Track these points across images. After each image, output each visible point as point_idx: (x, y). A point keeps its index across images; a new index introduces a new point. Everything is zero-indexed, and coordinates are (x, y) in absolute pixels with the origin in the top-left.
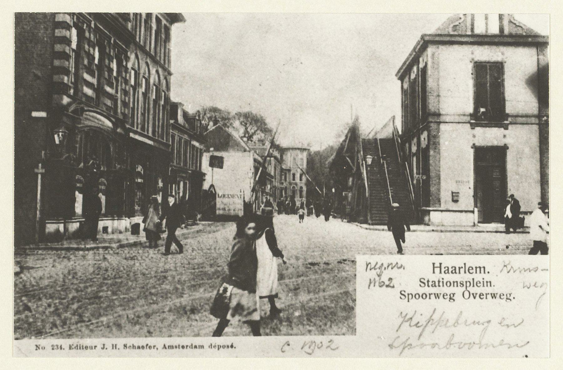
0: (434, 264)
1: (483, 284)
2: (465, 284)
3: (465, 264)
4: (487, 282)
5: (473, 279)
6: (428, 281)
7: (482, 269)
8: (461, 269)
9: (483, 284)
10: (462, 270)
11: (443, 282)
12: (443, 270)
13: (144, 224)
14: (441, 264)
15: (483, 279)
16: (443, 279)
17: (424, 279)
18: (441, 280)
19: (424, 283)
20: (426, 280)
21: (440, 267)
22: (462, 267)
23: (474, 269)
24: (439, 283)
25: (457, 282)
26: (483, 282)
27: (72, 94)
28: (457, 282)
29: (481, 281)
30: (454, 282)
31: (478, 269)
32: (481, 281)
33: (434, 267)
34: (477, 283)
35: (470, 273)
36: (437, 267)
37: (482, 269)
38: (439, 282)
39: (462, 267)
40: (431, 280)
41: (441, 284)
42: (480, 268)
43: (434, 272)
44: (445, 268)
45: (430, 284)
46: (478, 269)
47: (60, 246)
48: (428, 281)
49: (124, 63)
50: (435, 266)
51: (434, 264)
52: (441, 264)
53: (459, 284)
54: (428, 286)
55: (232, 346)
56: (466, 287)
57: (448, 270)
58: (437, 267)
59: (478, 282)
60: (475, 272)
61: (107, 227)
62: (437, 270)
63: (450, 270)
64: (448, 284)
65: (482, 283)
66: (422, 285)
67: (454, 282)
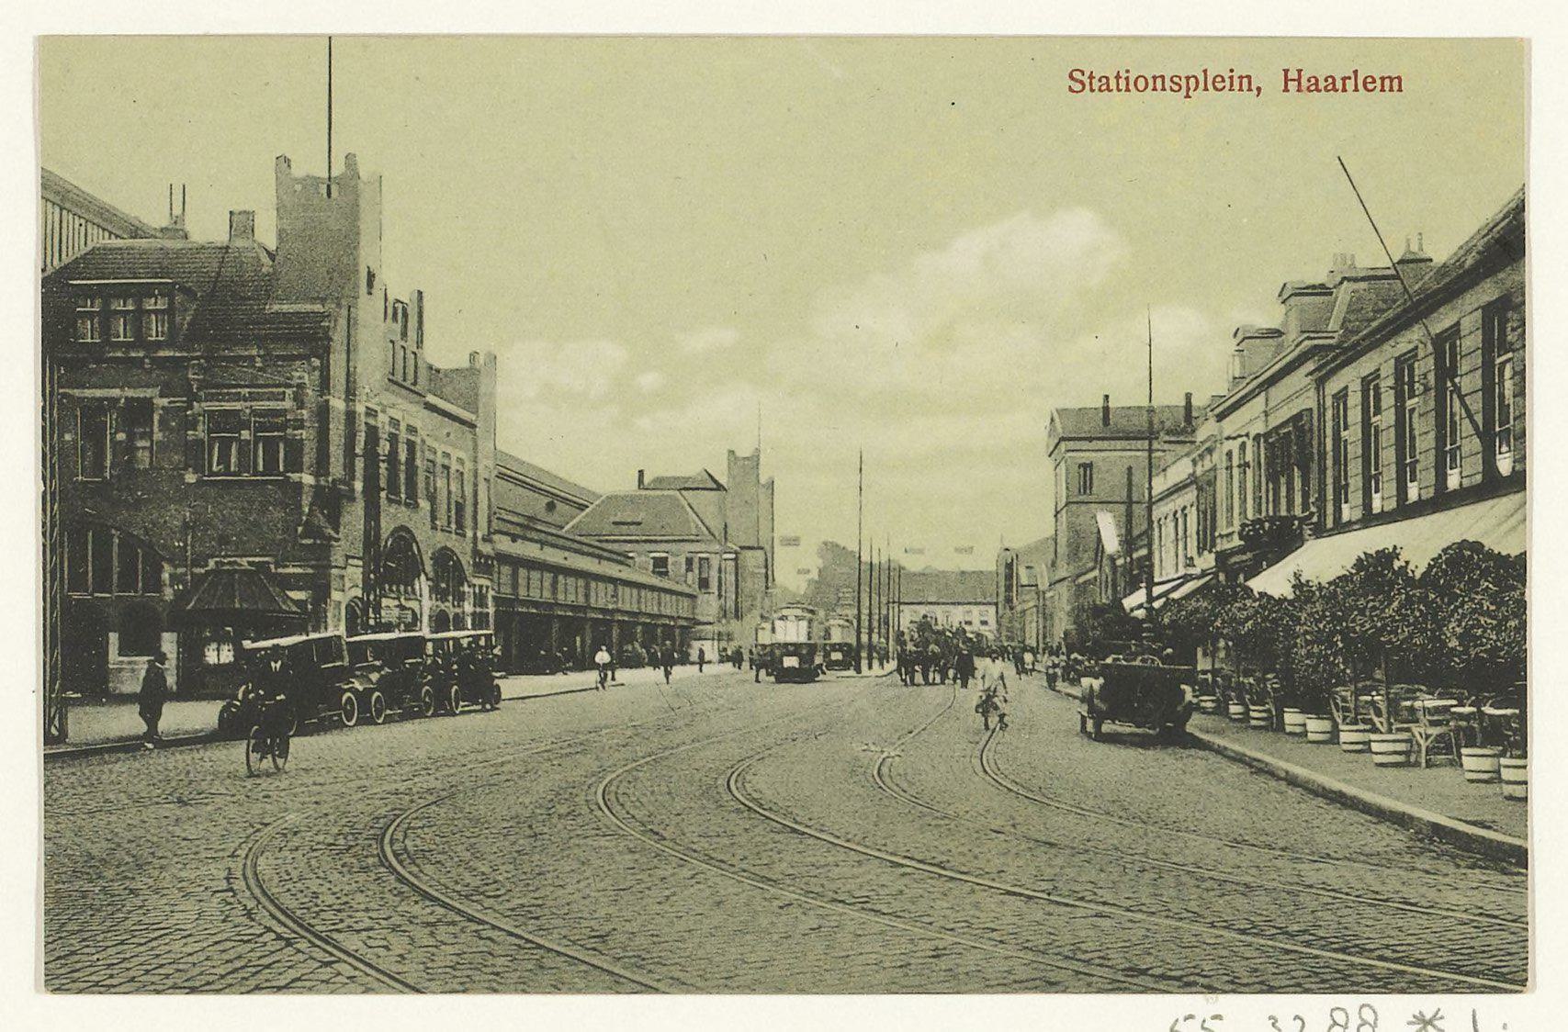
0: (1286, 71)
1: (1232, 85)
2: (1183, 83)
3: (1356, 72)
5: (1205, 71)
6: (1091, 77)
7: (1396, 81)
8: (1347, 81)
9: (1232, 85)
10: (1350, 84)
11: (1127, 78)
14: (1300, 71)
15: (1232, 71)
18: (1123, 75)
19: (1082, 82)
20: (1087, 74)
22: (1350, 78)
23: (1379, 82)
26: (1231, 78)
27: (1221, 640)
28: (1163, 77)
29: (1227, 75)
30: (1155, 78)
31: (1387, 82)
32: (1227, 75)
36: (1294, 80)
37: (1396, 81)
38: (1118, 77)
39: (1350, 78)
43: (1286, 90)
45: (1096, 85)
46: (1387, 82)
48: (1091, 77)
49: (291, 733)
51: (1286, 71)
52: (1300, 71)
53: (1168, 84)
54: (1119, 90)
55: (1420, 234)
56: (1188, 89)
57: (1334, 83)
58: (1294, 80)
59: (1219, 79)
60: (1379, 88)
62: (1293, 85)
64: (1141, 83)
66: (1078, 87)
67: (1155, 78)
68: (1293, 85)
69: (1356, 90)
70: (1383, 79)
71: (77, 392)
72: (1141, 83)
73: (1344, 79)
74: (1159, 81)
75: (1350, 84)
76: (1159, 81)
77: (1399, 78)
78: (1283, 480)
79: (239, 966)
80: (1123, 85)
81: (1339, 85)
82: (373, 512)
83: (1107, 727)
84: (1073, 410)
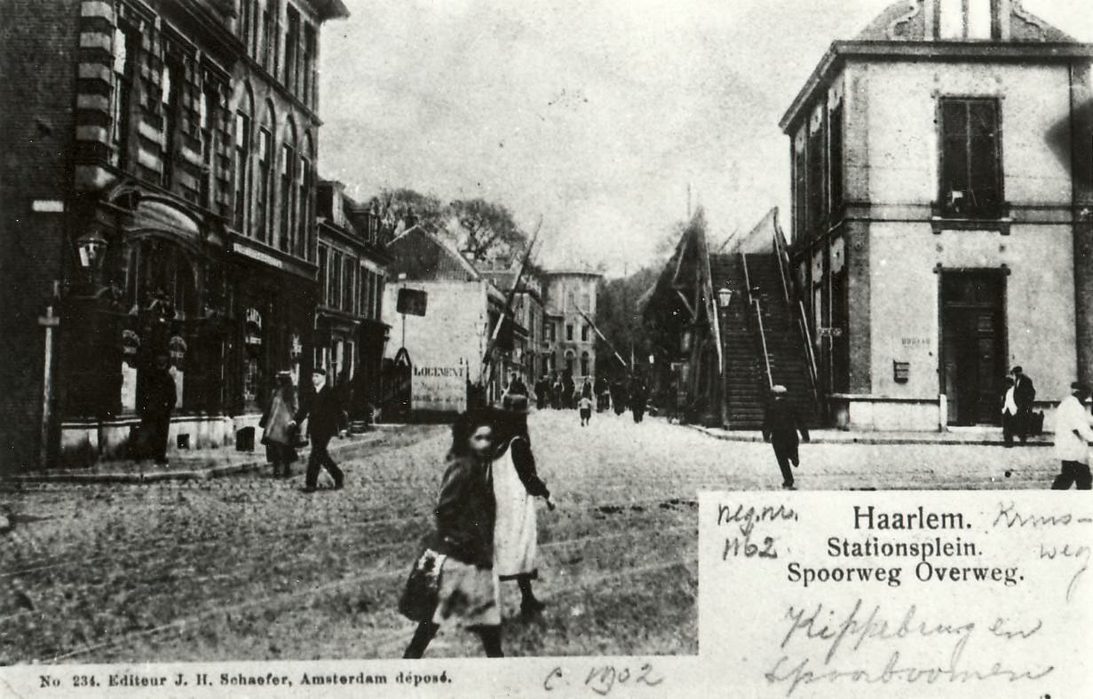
0: (857, 509)
3: (921, 509)
4: (966, 546)
5: (938, 540)
6: (846, 544)
7: (956, 520)
10: (915, 522)
11: (876, 546)
12: (876, 521)
13: (262, 430)
14: (871, 509)
15: (959, 539)
16: (876, 539)
17: (838, 540)
18: (872, 542)
19: (837, 548)
20: (842, 541)
21: (870, 516)
22: (915, 516)
24: (867, 549)
25: (904, 545)
26: (959, 545)
28: (904, 545)
30: (898, 546)
31: (948, 520)
33: (857, 516)
34: (945, 548)
35: (931, 527)
37: (956, 520)
38: (868, 545)
39: (915, 516)
40: (851, 542)
41: (872, 550)
42: (952, 516)
43: (857, 526)
44: (880, 517)
45: (850, 549)
46: (948, 520)
47: (91, 475)
48: (846, 544)
50: (860, 512)
51: (857, 509)
52: (871, 509)
53: (909, 550)
59: (932, 518)
61: (187, 436)
62: (864, 522)
63: (891, 521)
64: (887, 550)
65: (955, 547)
66: (834, 551)
67: (898, 546)
68: (864, 522)
69: (921, 526)
70: (944, 516)
71: (969, 159)
72: (887, 550)
73: (910, 517)
74: (902, 549)
75: (915, 522)
76: (902, 549)
77: (960, 516)
78: (516, 332)
79: (535, 322)
80: (872, 550)
81: (905, 523)
82: (1082, 360)
83: (1029, 440)
84: (868, 367)
